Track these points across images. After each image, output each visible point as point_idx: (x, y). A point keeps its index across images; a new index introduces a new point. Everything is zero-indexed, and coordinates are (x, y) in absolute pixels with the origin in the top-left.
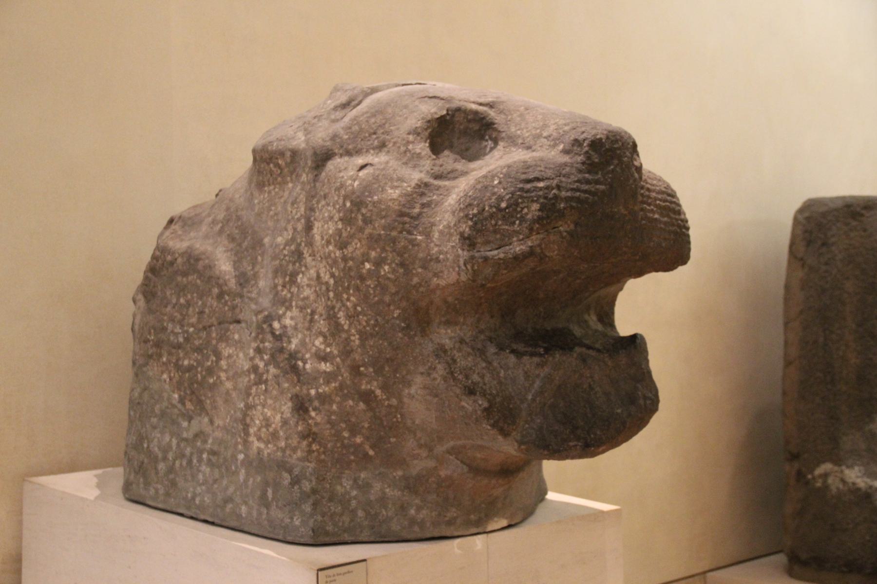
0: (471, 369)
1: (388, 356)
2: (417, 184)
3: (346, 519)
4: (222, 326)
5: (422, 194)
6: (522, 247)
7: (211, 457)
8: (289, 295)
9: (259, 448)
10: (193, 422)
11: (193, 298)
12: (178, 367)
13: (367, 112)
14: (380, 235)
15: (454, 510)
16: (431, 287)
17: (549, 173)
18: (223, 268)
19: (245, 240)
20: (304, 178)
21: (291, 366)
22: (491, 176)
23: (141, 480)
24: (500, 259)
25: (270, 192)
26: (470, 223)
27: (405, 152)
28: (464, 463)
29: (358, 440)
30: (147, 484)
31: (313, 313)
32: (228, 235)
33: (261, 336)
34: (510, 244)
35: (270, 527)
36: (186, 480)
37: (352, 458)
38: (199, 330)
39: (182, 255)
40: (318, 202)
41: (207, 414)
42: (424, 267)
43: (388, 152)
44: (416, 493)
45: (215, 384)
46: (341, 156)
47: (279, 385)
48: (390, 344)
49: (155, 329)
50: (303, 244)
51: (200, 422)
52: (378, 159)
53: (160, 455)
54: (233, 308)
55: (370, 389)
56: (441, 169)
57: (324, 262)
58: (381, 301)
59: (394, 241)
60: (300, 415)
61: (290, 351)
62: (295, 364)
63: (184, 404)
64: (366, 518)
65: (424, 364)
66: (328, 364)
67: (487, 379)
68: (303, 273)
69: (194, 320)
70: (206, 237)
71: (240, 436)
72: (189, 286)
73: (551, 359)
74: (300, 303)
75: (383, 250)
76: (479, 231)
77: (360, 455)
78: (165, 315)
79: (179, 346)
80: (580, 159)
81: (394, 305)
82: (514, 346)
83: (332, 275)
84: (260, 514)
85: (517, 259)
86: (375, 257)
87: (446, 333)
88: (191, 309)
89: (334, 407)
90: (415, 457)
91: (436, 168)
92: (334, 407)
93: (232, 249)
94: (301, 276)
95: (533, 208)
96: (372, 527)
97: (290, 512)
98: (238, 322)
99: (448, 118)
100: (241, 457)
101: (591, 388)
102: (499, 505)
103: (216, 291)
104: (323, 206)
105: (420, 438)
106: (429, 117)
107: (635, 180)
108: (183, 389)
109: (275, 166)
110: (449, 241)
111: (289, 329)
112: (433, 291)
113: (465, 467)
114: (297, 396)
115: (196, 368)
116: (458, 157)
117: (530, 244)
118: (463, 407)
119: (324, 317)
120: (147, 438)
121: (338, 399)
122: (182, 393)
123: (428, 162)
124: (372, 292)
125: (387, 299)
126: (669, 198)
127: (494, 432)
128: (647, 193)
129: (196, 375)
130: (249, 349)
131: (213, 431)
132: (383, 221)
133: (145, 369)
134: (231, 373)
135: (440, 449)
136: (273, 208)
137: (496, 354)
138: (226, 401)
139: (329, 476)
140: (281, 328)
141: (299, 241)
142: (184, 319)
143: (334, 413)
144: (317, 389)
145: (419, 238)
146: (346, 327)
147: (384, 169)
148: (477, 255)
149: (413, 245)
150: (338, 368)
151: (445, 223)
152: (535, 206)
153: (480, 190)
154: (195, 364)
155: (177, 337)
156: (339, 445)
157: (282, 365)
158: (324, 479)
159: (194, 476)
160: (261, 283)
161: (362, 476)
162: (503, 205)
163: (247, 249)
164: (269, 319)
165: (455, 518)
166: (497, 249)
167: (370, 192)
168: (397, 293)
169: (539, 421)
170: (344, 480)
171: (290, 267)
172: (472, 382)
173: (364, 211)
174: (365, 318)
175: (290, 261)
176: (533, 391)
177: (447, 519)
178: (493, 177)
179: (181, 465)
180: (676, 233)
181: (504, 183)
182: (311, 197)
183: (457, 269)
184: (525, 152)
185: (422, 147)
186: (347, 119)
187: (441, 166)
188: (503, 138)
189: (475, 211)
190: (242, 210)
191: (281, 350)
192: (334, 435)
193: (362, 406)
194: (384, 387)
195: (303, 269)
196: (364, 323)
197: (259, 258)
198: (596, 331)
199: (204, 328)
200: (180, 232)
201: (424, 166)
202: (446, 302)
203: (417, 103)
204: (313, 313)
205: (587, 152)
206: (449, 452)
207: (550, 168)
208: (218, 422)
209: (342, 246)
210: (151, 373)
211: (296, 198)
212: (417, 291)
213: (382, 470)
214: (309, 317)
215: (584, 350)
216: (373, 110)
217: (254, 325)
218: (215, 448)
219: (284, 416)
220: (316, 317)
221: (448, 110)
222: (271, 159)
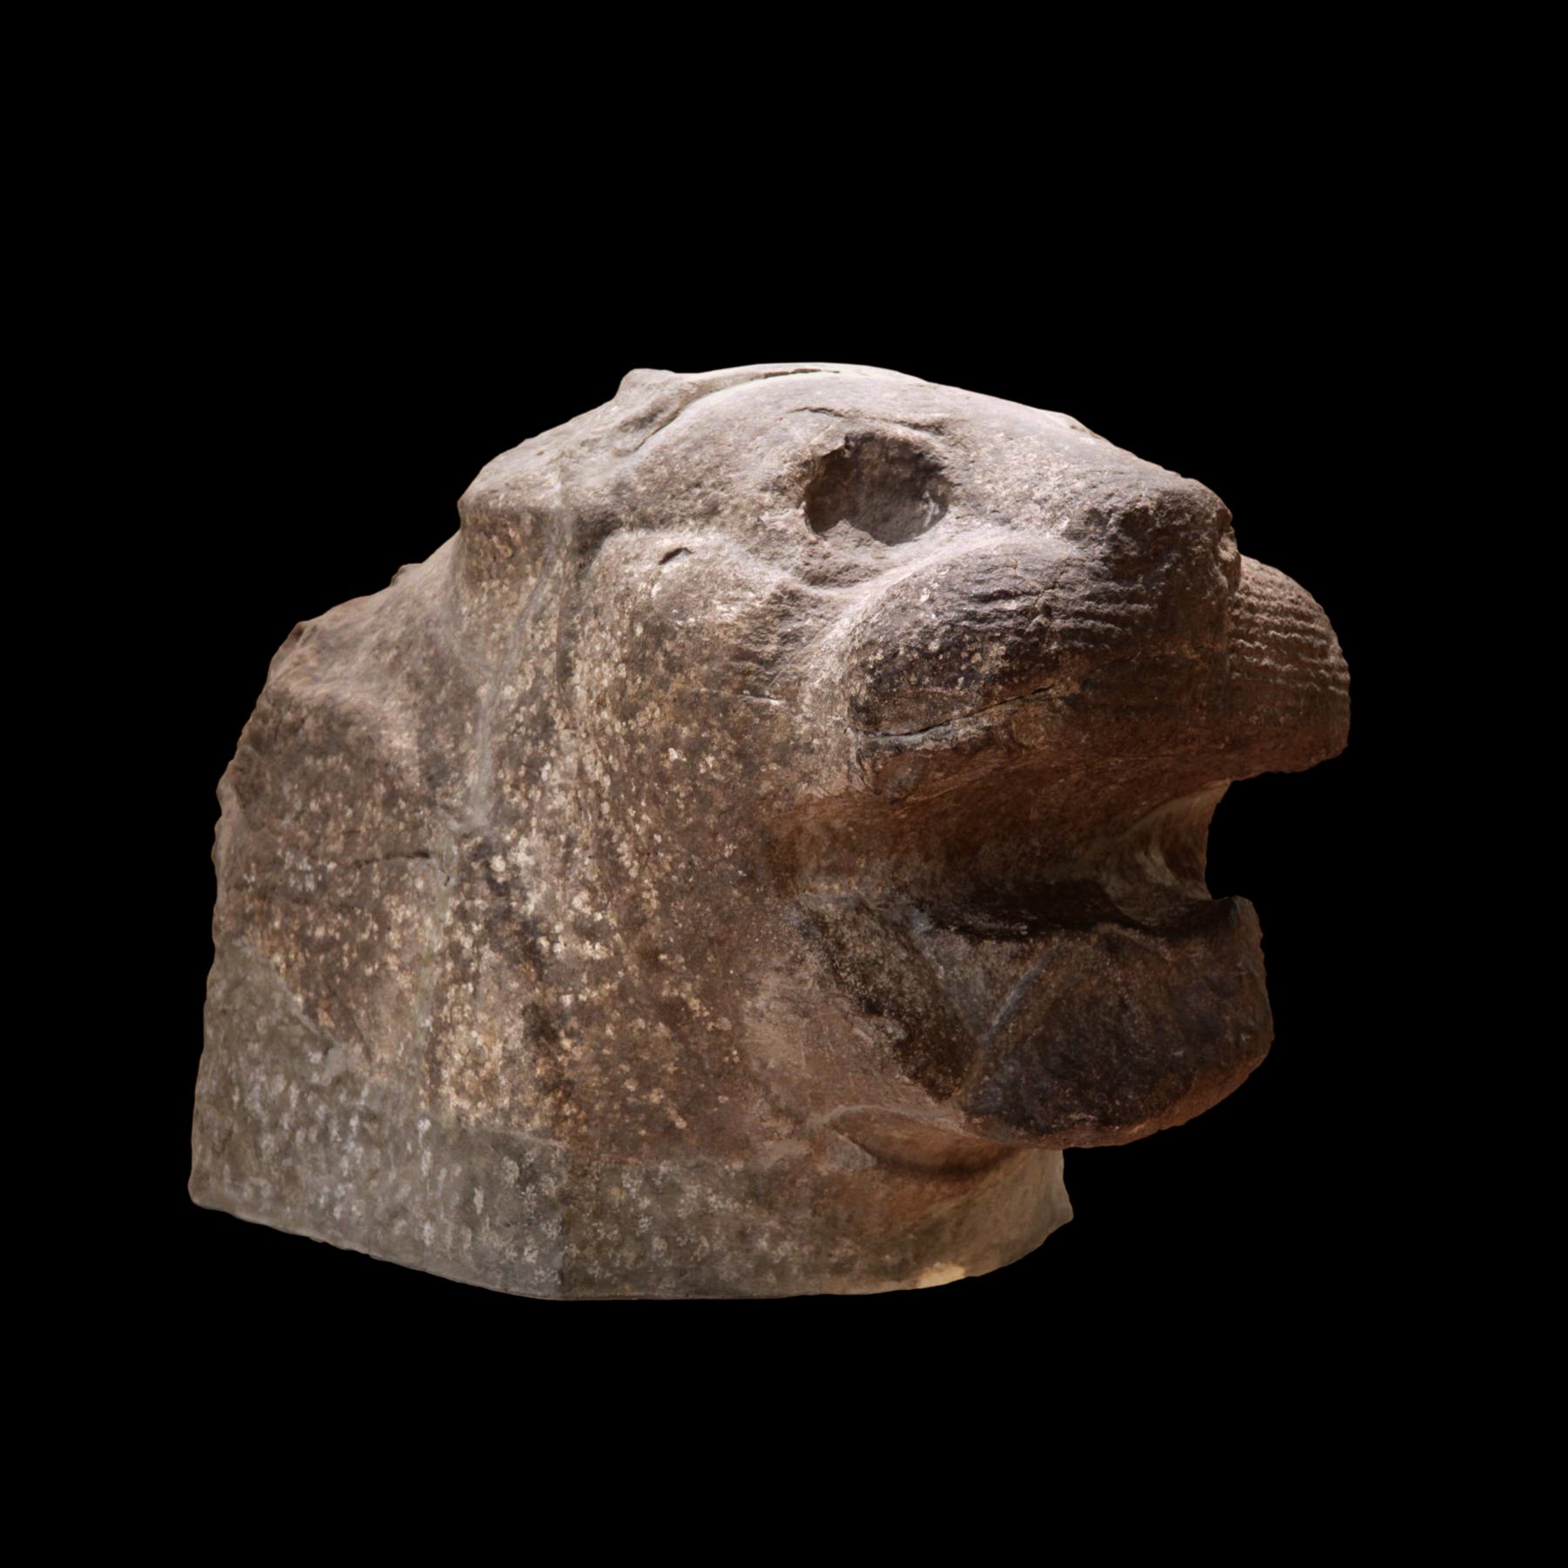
0: (876, 962)
1: (712, 934)
2: (774, 595)
3: (629, 1254)
4: (392, 861)
5: (785, 615)
6: (968, 728)
7: (366, 1125)
8: (525, 805)
9: (458, 1109)
10: (331, 1052)
11: (335, 800)
12: (304, 941)
13: (684, 439)
14: (698, 695)
15: (848, 1242)
16: (797, 801)
17: (1031, 582)
18: (397, 743)
20: (558, 568)
21: (526, 946)
22: (913, 586)
23: (227, 1167)
24: (926, 751)
25: (491, 593)
26: (869, 680)
27: (755, 527)
28: (869, 1151)
29: (655, 1097)
30: (238, 1177)
31: (570, 842)
32: (409, 675)
33: (466, 886)
34: (948, 722)
35: (479, 1266)
36: (316, 1170)
37: (643, 1132)
38: (347, 868)
39: (316, 711)
40: (583, 621)
41: (361, 1039)
42: (783, 761)
43: (723, 524)
44: (770, 1206)
45: (375, 978)
46: (632, 527)
47: (499, 984)
48: (717, 909)
49: (258, 863)
50: (554, 704)
51: (346, 1054)
52: (699, 540)
53: (265, 1120)
54: (415, 826)
55: (679, 998)
56: (826, 563)
57: (592, 741)
58: (699, 825)
59: (725, 707)
60: (539, 1046)
61: (523, 917)
62: (534, 943)
63: (314, 1016)
64: (668, 1255)
65: (782, 951)
66: (598, 946)
67: (906, 984)
68: (552, 761)
69: (336, 847)
70: (365, 677)
71: (424, 1085)
72: (328, 778)
73: (1040, 946)
74: (546, 822)
75: (705, 724)
76: (884, 696)
77: (660, 1130)
78: (279, 833)
79: (305, 899)
80: (1099, 550)
82: (970, 920)
83: (608, 770)
84: (459, 1240)
85: (963, 753)
86: (688, 738)
87: (830, 891)
88: (331, 824)
89: (609, 1031)
90: (769, 1134)
91: (815, 562)
92: (609, 1031)
93: (415, 705)
94: (548, 767)
95: (992, 654)
96: (681, 1273)
97: (516, 1238)
98: (425, 855)
99: (847, 454)
100: (424, 1125)
101: (1124, 1006)
102: (946, 1237)
103: (381, 789)
104: (593, 630)
105: (778, 1097)
106: (807, 455)
107: (1219, 590)
108: (313, 986)
109: (502, 542)
110: (830, 711)
111: (523, 873)
112: (802, 808)
113: (868, 1157)
114: (535, 1007)
115: (340, 944)
116: (865, 535)
117: (985, 722)
118: (857, 1037)
119: (591, 852)
120: (240, 1084)
121: (616, 1015)
122: (311, 995)
123: (800, 548)
124: (682, 807)
125: (711, 820)
126: (1299, 623)
127: (918, 1089)
128: (1248, 615)
129: (340, 960)
130: (444, 910)
131: (372, 1073)
132: (705, 667)
133: (237, 943)
134: (408, 958)
135: (818, 1120)
136: (497, 626)
137: (928, 933)
138: (398, 1013)
139: (596, 1167)
140: (507, 869)
141: (545, 695)
142: (317, 844)
143: (606, 1042)
144: (576, 994)
145: (775, 703)
146: (633, 873)
147: (711, 561)
148: (881, 741)
149: (763, 718)
150: (617, 953)
151: (825, 676)
152: (998, 649)
153: (891, 615)
154: (338, 936)
155: (303, 881)
156: (616, 1107)
157: (506, 945)
158: (585, 1174)
159: (331, 1163)
160: (472, 778)
161: (663, 1169)
162: (934, 646)
163: (444, 707)
164: (484, 852)
165: (852, 1260)
166: (922, 731)
167: (681, 609)
168: (731, 810)
169: (1011, 1069)
170: (625, 1177)
171: (528, 749)
172: (875, 991)
173: (668, 645)
174: (669, 858)
175: (527, 737)
176: (1003, 1009)
177: (834, 1260)
178: (919, 588)
179: (306, 1139)
180: (1312, 695)
181: (940, 602)
182: (569, 609)
183: (845, 767)
184: (998, 529)
185: (790, 518)
186: (645, 452)
187: (825, 557)
188: (957, 499)
189: (879, 657)
190: (437, 624)
191: (507, 915)
192: (608, 1086)
193: (662, 1029)
194: (706, 994)
195: (553, 754)
196: (668, 868)
197: (469, 726)
198: (1160, 887)
199: (358, 864)
200: (312, 663)
201: (790, 557)
202: (827, 827)
203: (785, 422)
204: (570, 842)
205: (1114, 538)
206: (834, 1126)
207: (1033, 572)
208: (382, 1055)
209: (627, 712)
210: (249, 952)
211: (543, 609)
212: (769, 807)
213: (702, 1158)
214: (562, 851)
215: (1115, 928)
216: (697, 435)
217: (455, 862)
218: (375, 1107)
219: (510, 1047)
220: (576, 851)
221: (847, 439)
222: (493, 525)
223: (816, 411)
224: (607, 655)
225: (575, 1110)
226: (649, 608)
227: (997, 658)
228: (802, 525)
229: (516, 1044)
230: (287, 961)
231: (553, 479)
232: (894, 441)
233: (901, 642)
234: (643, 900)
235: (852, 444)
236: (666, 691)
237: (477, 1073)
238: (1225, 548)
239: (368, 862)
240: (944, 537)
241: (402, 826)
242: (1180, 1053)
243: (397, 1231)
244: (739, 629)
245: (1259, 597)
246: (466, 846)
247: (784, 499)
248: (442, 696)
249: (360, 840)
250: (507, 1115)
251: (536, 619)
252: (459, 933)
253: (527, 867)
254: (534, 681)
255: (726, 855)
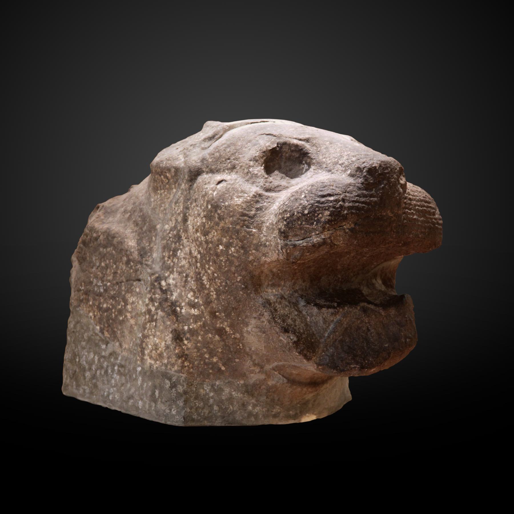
0: (287, 315)
1: (233, 306)
2: (254, 195)
3: (206, 411)
4: (129, 282)
5: (257, 202)
6: (317, 239)
7: (120, 369)
8: (172, 264)
9: (150, 363)
10: (109, 345)
11: (110, 262)
12: (100, 309)
13: (224, 144)
14: (229, 228)
15: (278, 407)
16: (261, 263)
17: (338, 191)
18: (130, 244)
20: (183, 186)
21: (172, 310)
22: (299, 192)
23: (74, 383)
24: (303, 246)
25: (161, 194)
26: (285, 223)
27: (248, 173)
28: (285, 377)
29: (215, 360)
30: (78, 386)
31: (187, 276)
32: (134, 221)
33: (153, 290)
34: (311, 237)
35: (157, 415)
36: (104, 384)
37: (211, 371)
38: (114, 285)
39: (103, 233)
40: (191, 204)
41: (118, 341)
42: (257, 250)
43: (237, 172)
44: (253, 395)
45: (123, 320)
46: (207, 173)
47: (164, 323)
48: (235, 298)
49: (85, 283)
50: (182, 231)
51: (113, 345)
52: (229, 177)
53: (87, 367)
54: (136, 271)
55: (223, 327)
56: (271, 185)
57: (194, 243)
58: (229, 271)
59: (238, 232)
60: (177, 343)
61: (172, 301)
62: (175, 309)
63: (103, 333)
64: (219, 411)
65: (256, 312)
66: (196, 310)
67: (297, 323)
68: (181, 250)
69: (110, 278)
70: (120, 222)
71: (139, 356)
72: (108, 255)
73: (341, 310)
74: (179, 269)
75: (231, 237)
76: (290, 228)
77: (216, 370)
78: (92, 273)
79: (100, 295)
80: (360, 180)
82: (318, 301)
83: (199, 252)
84: (150, 406)
85: (316, 247)
86: (226, 242)
87: (272, 292)
88: (109, 270)
89: (200, 338)
90: (252, 372)
91: (267, 184)
92: (200, 338)
93: (136, 231)
94: (180, 251)
95: (325, 214)
96: (223, 417)
97: (169, 406)
98: (139, 280)
99: (278, 149)
100: (139, 369)
101: (368, 330)
102: (310, 405)
103: (125, 259)
104: (194, 207)
105: (255, 360)
106: (265, 149)
107: (400, 193)
108: (102, 323)
109: (164, 178)
110: (272, 233)
111: (171, 286)
112: (263, 265)
113: (285, 379)
114: (175, 330)
115: (111, 310)
116: (284, 175)
117: (323, 237)
118: (281, 340)
119: (194, 279)
120: (79, 355)
121: (202, 333)
122: (102, 326)
123: (262, 180)
124: (224, 264)
125: (233, 269)
126: (426, 204)
127: (301, 357)
128: (409, 202)
129: (111, 315)
130: (145, 298)
131: (122, 352)
132: (231, 219)
133: (78, 309)
134: (134, 314)
135: (268, 367)
136: (163, 205)
137: (304, 306)
138: (130, 332)
139: (195, 382)
140: (166, 285)
141: (179, 228)
142: (104, 277)
143: (199, 342)
144: (189, 326)
145: (254, 230)
146: (208, 286)
147: (233, 184)
148: (289, 243)
149: (250, 235)
150: (202, 312)
151: (270, 221)
152: (327, 213)
153: (292, 201)
154: (111, 307)
155: (99, 289)
156: (202, 363)
157: (166, 310)
158: (192, 385)
159: (109, 381)
160: (155, 255)
161: (217, 383)
162: (306, 212)
163: (145, 232)
164: (158, 279)
165: (279, 413)
166: (302, 240)
167: (223, 200)
168: (239, 265)
169: (331, 350)
170: (205, 386)
171: (173, 246)
172: (287, 325)
173: (219, 212)
174: (219, 281)
175: (173, 242)
176: (329, 331)
177: (273, 413)
178: (301, 193)
179: (100, 373)
180: (430, 228)
181: (308, 197)
182: (187, 200)
183: (277, 252)
184: (327, 173)
185: (259, 170)
186: (211, 148)
187: (271, 183)
188: (314, 163)
189: (288, 215)
190: (143, 205)
191: (166, 300)
192: (199, 356)
193: (217, 337)
194: (231, 326)
195: (181, 247)
196: (219, 284)
197: (154, 238)
198: (380, 291)
199: (117, 283)
200: (102, 217)
201: (259, 182)
202: (271, 271)
203: (257, 138)
204: (187, 276)
205: (365, 176)
206: (273, 369)
207: (339, 187)
208: (125, 346)
209: (205, 233)
210: (82, 312)
211: (178, 200)
212: (252, 265)
213: (230, 379)
214: (184, 279)
215: (366, 304)
216: (228, 143)
217: (149, 283)
218: (123, 363)
219: (167, 343)
220: (189, 279)
221: (278, 144)
222: (162, 172)
223: (267, 135)
224: (199, 215)
225: (188, 364)
226: (213, 199)
227: (327, 216)
228: (263, 172)
229: (169, 342)
230: (94, 315)
231: (181, 157)
232: (293, 144)
233: (295, 210)
234: (211, 295)
235: (279, 145)
236: (218, 226)
237: (156, 352)
238: (402, 180)
239: (120, 283)
240: (310, 176)
241: (132, 271)
242: (387, 345)
244: (242, 206)
245: (413, 196)
246: (153, 277)
247: (257, 163)
248: (145, 228)
249: (118, 275)
250: (166, 366)
251: (176, 203)
252: (151, 306)
253: (173, 284)
254: (175, 223)
255: (238, 280)
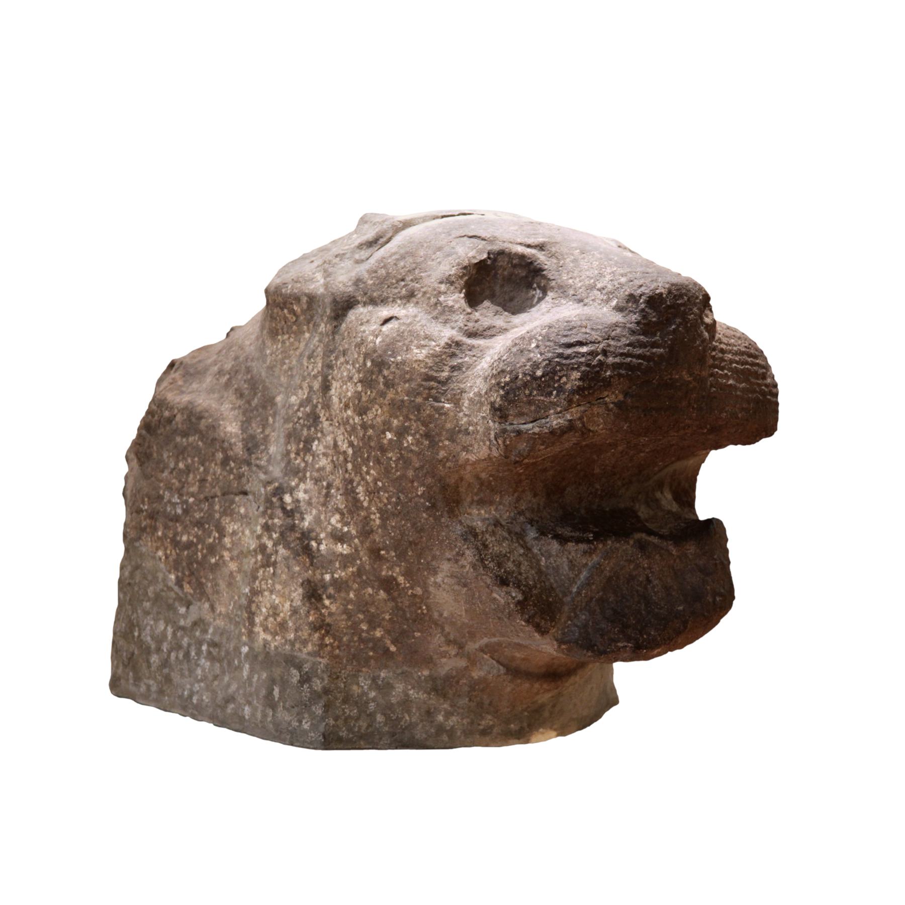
0: (505, 555)
1: (411, 539)
2: (447, 344)
3: (363, 724)
4: (226, 497)
5: (453, 355)
6: (559, 420)
7: (211, 649)
8: (303, 465)
9: (265, 640)
10: (191, 607)
11: (193, 462)
12: (175, 543)
13: (395, 253)
14: (403, 401)
15: (489, 717)
16: (460, 462)
17: (595, 336)
18: (229, 429)
19: (255, 398)
20: (322, 328)
21: (304, 546)
22: (527, 338)
23: (131, 674)
24: (534, 434)
25: (283, 342)
26: (502, 392)
27: (436, 304)
28: (502, 664)
29: (378, 633)
30: (137, 679)
31: (329, 486)
32: (236, 390)
33: (269, 511)
34: (547, 417)
35: (277, 731)
36: (182, 675)
37: (371, 654)
38: (200, 501)
39: (182, 410)
40: (337, 358)
41: (209, 600)
42: (452, 439)
43: (417, 303)
44: (445, 696)
45: (217, 564)
46: (365, 304)
47: (288, 568)
48: (414, 525)
49: (149, 498)
50: (320, 406)
51: (200, 608)
52: (403, 311)
53: (153, 646)
54: (240, 477)
55: (392, 576)
56: (476, 325)
57: (342, 428)
58: (403, 476)
59: (418, 408)
60: (311, 604)
61: (302, 529)
62: (308, 544)
63: (181, 587)
64: (386, 724)
65: (451, 549)
66: (345, 546)
67: (523, 568)
68: (319, 439)
69: (194, 489)
70: (211, 391)
71: (245, 626)
72: (189, 449)
73: (601, 546)
74: (315, 474)
75: (407, 418)
76: (510, 402)
77: (381, 652)
78: (161, 481)
79: (176, 519)
80: (635, 317)
81: (419, 482)
82: (560, 531)
83: (351, 444)
84: (265, 716)
85: (556, 434)
86: (397, 426)
87: (479, 514)
88: (191, 476)
89: (352, 595)
90: (444, 655)
91: (470, 325)
92: (352, 595)
93: (240, 407)
94: (316, 442)
95: (573, 378)
97: (298, 714)
98: (245, 493)
99: (489, 262)
100: (245, 649)
101: (648, 581)
102: (546, 714)
103: (220, 456)
104: (342, 364)
105: (449, 633)
106: (466, 263)
107: (704, 341)
108: (180, 569)
109: (290, 313)
110: (479, 410)
111: (302, 504)
112: (463, 467)
113: (501, 668)
114: (309, 581)
115: (196, 545)
116: (499, 309)
117: (569, 417)
118: (495, 599)
119: (341, 492)
120: (138, 626)
121: (356, 586)
122: (180, 574)
123: (462, 317)
124: (394, 466)
125: (410, 473)
126: (750, 360)
127: (530, 628)
128: (720, 355)
129: (196, 554)
130: (256, 525)
131: (214, 619)
132: (407, 385)
133: (137, 544)
134: (235, 553)
135: (472, 647)
136: (287, 361)
137: (536, 539)
138: (230, 585)
139: (344, 673)
140: (293, 502)
141: (315, 401)
142: (183, 487)
143: (350, 601)
144: (332, 573)
145: (447, 405)
146: (365, 504)
147: (410, 324)
148: (508, 428)
149: (440, 414)
150: (356, 550)
151: (476, 390)
152: (576, 375)
153: (514, 355)
154: (195, 540)
155: (175, 508)
156: (356, 639)
157: (292, 545)
158: (338, 677)
159: (191, 671)
160: (272, 449)
161: (383, 675)
162: (539, 373)
163: (256, 408)
164: (279, 492)
165: (492, 727)
166: (532, 422)
167: (393, 352)
168: (422, 467)
169: (584, 617)
170: (361, 679)
171: (305, 432)
172: (505, 572)
173: (386, 372)
174: (386, 495)
175: (304, 425)
176: (579, 583)
177: (481, 727)
178: (530, 339)
179: (177, 658)
180: (757, 401)
181: (542, 347)
182: (329, 352)
183: (488, 443)
184: (576, 305)
185: (456, 299)
186: (372, 261)
187: (476, 321)
188: (553, 288)
189: (507, 379)
190: (252, 360)
191: (293, 528)
192: (351, 627)
193: (382, 594)
194: (407, 574)
195: (319, 435)
196: (385, 501)
197: (270, 419)
198: (669, 512)
199: (206, 499)
200: (180, 383)
201: (456, 321)
202: (477, 477)
203: (453, 244)
204: (329, 486)
205: (643, 310)
206: (482, 650)
207: (596, 330)
208: (220, 609)
209: (362, 411)
210: (144, 549)
211: (314, 351)
212: (444, 466)
213: (405, 668)
214: (324, 491)
215: (644, 535)
216: (402, 251)
217: (263, 498)
218: (217, 639)
219: (294, 605)
220: (333, 491)
221: (489, 253)
222: (285, 303)
223: (471, 237)
224: (350, 378)
225: (332, 641)
226: (375, 351)
227: (576, 380)
228: (463, 303)
229: (298, 603)
230: (166, 555)
231: (319, 276)
232: (516, 254)
233: (520, 371)
234: (371, 519)
235: (492, 256)
236: (384, 399)
237: (275, 619)
238: (707, 317)
239: (212, 497)
240: (545, 310)
241: (232, 477)
242: (681, 608)
243: (229, 711)
244: (427, 363)
245: (727, 345)
246: (269, 488)
247: (452, 288)
248: (255, 402)
249: (208, 485)
250: (292, 644)
251: (310, 357)
252: (265, 538)
253: (304, 500)
254: (308, 393)
255: (419, 493)
